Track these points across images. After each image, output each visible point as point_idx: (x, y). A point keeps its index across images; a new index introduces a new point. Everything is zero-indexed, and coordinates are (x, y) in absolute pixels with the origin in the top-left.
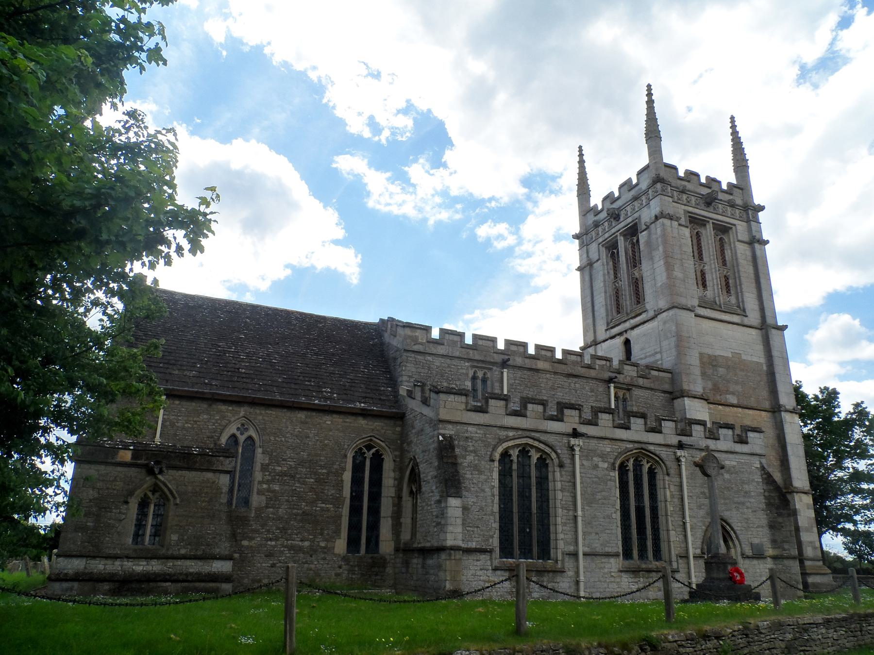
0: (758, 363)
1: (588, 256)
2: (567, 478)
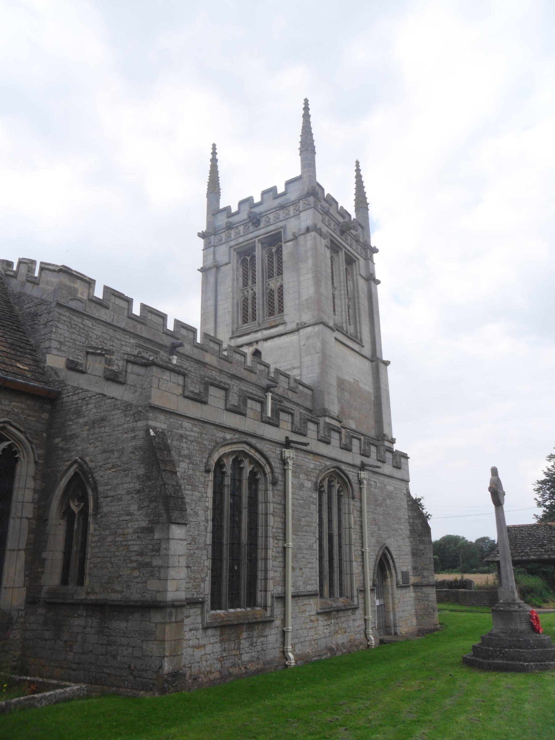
0: (369, 392)
1: (214, 258)
2: (278, 499)
